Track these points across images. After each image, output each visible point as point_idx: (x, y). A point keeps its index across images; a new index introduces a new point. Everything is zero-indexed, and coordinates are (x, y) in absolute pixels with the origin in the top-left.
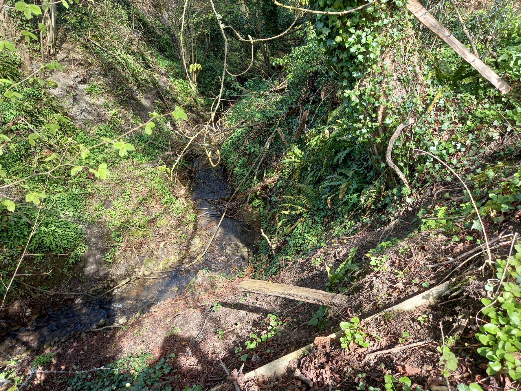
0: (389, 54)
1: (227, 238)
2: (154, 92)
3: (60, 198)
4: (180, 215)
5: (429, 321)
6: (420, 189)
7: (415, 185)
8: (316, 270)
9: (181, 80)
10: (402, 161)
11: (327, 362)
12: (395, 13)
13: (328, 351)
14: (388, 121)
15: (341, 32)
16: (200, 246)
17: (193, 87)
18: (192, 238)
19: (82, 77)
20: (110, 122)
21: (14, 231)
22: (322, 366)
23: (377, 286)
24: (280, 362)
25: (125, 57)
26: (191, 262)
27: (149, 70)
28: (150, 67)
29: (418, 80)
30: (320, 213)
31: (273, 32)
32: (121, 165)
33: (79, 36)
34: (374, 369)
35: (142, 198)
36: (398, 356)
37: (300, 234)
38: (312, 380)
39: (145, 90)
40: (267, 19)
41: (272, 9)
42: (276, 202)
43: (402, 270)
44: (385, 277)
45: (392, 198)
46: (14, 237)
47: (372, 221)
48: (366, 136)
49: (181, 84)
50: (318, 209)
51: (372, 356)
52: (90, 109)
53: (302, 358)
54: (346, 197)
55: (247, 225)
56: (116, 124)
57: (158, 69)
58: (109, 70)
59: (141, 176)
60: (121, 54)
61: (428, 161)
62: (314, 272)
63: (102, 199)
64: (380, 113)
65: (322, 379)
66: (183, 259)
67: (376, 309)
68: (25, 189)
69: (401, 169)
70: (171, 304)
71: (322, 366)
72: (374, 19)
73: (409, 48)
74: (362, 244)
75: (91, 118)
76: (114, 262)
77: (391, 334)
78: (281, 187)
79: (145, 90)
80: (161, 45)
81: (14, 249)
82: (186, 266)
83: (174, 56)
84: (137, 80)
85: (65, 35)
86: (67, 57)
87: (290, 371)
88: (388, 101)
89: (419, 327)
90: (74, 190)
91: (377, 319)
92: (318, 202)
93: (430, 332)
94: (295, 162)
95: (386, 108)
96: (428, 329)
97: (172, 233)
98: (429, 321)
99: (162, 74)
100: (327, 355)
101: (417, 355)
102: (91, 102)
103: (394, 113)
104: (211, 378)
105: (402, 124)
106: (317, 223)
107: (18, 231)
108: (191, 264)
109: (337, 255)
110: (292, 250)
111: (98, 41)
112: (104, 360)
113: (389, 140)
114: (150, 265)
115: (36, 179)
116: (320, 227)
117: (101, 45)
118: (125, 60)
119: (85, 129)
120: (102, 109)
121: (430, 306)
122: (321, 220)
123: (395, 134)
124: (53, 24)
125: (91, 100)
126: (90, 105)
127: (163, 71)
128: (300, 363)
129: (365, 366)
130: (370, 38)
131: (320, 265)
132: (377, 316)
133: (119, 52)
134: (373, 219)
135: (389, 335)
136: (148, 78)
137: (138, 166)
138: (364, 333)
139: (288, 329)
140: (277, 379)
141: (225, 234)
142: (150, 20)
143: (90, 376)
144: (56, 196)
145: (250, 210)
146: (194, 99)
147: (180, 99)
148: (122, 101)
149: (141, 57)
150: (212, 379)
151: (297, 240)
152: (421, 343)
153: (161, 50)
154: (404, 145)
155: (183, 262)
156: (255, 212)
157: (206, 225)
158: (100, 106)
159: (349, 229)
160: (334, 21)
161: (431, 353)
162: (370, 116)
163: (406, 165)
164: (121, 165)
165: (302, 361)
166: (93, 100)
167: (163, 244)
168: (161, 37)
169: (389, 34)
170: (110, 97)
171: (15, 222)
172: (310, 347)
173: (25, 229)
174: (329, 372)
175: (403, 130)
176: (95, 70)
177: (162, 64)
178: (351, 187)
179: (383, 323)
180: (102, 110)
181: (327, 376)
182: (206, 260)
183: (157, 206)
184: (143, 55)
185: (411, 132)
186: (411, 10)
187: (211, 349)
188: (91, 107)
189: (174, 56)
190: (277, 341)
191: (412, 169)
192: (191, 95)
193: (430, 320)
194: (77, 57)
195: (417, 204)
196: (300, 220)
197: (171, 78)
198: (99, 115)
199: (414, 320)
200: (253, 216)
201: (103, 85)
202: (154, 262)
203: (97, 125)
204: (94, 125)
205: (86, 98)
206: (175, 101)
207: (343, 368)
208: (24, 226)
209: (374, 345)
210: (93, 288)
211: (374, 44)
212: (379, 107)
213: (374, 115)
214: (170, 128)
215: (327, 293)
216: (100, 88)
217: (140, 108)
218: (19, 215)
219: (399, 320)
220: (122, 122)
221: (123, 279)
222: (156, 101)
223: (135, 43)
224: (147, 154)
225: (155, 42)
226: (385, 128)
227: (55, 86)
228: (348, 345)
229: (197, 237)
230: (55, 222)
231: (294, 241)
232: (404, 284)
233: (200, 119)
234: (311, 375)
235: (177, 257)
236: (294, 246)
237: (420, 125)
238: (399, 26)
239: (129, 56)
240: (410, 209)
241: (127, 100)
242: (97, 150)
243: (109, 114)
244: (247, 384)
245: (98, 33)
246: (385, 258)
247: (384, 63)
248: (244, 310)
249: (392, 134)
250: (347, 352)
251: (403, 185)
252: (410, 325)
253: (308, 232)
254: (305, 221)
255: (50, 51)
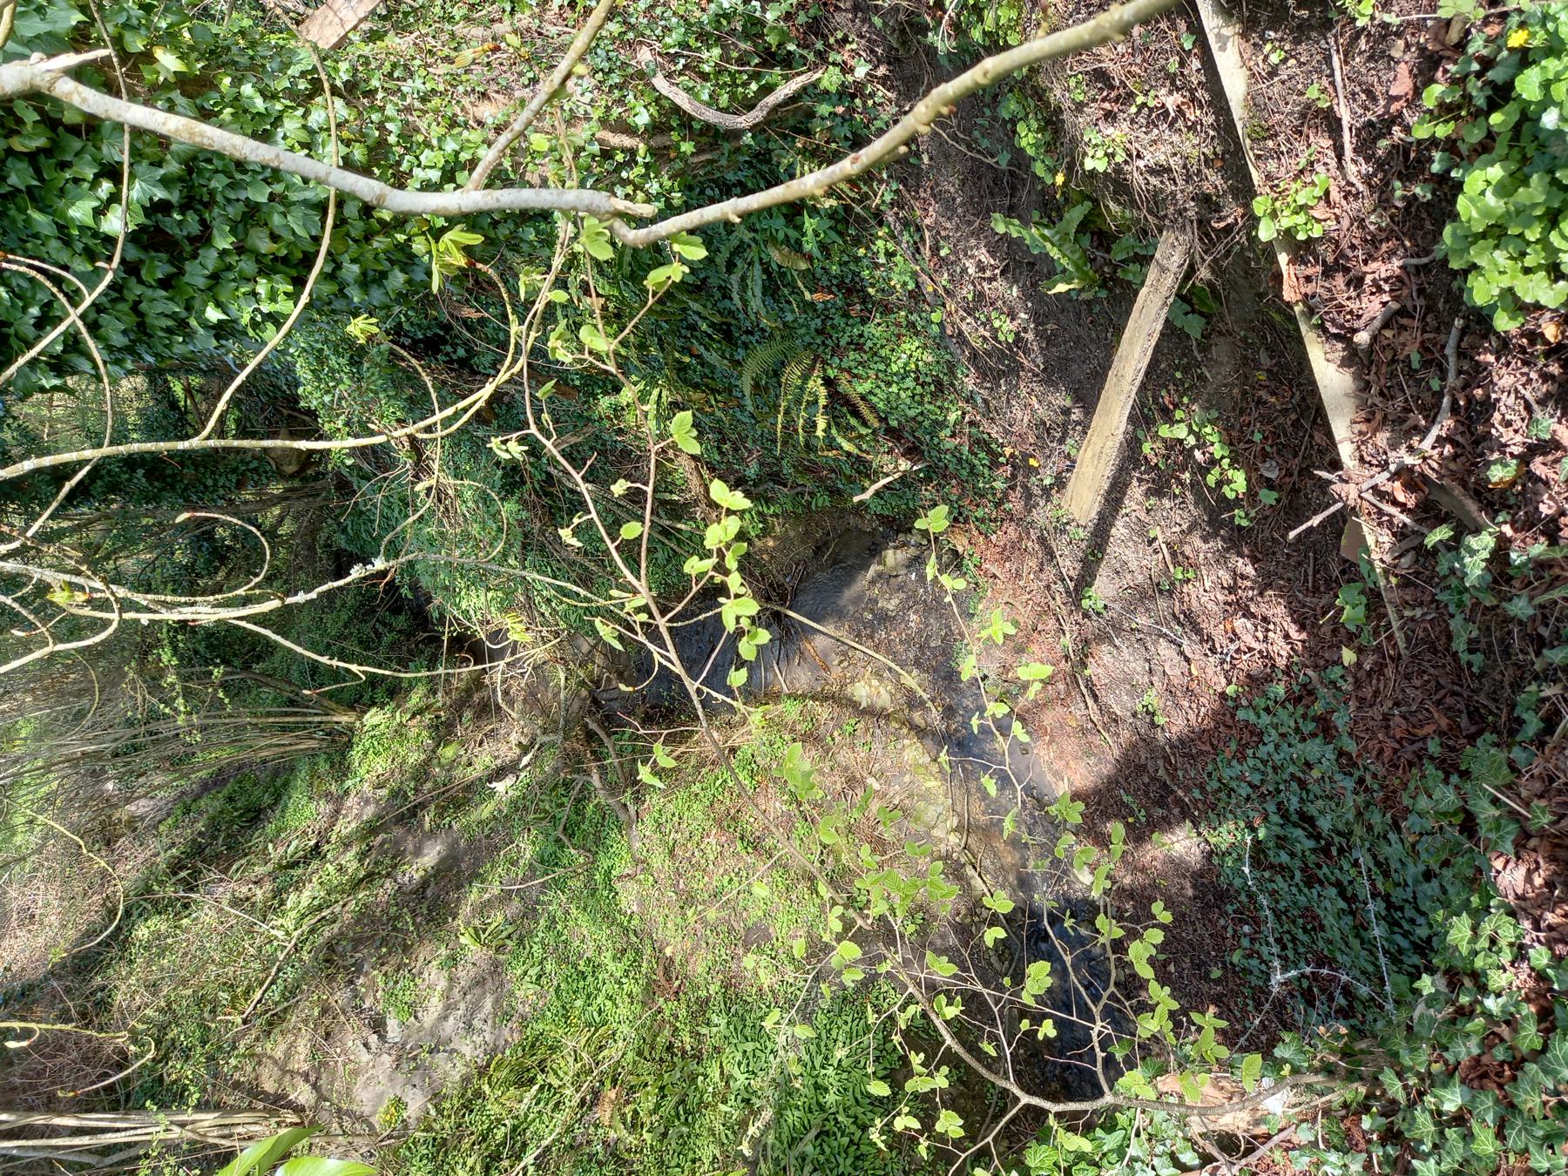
0: (468, 106)
1: (851, 608)
2: (398, 831)
3: (739, 1064)
4: (787, 737)
5: (1282, 40)
6: (832, 40)
7: (819, 54)
8: (1025, 330)
9: (356, 754)
10: (745, 84)
11: (1346, 270)
12: (363, 85)
13: (1319, 269)
14: (642, 119)
15: (401, 238)
16: (875, 683)
17: (375, 721)
18: (854, 705)
19: (366, 1032)
20: (500, 949)
21: (841, 1169)
22: (1357, 282)
23: (1163, 157)
24: (1327, 382)
25: (293, 914)
26: (922, 703)
27: (326, 847)
28: (317, 846)
29: (528, 30)
30: (833, 327)
31: (213, 472)
32: (635, 908)
33: (235, 1048)
34: (1380, 165)
35: (739, 843)
36: (1360, 111)
37: (889, 384)
38: (1384, 304)
39: (394, 857)
40: (173, 488)
41: (141, 472)
42: (761, 464)
43: (1131, 95)
44: (1142, 136)
45: (839, 120)
46: (855, 1169)
47: (890, 177)
48: (668, 184)
49: (365, 754)
50: (819, 332)
51: (1351, 169)
52: (462, 1006)
53: (1325, 330)
54: (807, 247)
55: (816, 553)
56: (505, 934)
57: (322, 824)
58: (336, 959)
59: (671, 853)
60: (284, 928)
61: (758, 14)
62: (1030, 336)
63: (741, 952)
64: (616, 140)
65: (1386, 280)
66: (914, 727)
67: (1231, 160)
68: (715, 1157)
69: (768, 89)
70: (1050, 742)
71: (1357, 282)
72: (382, 143)
73: (446, 51)
74: (963, 204)
75: (488, 1003)
76: (920, 908)
77: (1302, 125)
78: (719, 448)
79: (394, 857)
80: (241, 815)
81: (889, 1169)
82: (935, 716)
83: (273, 780)
84: (356, 884)
85: (237, 1085)
86: (306, 1077)
87: (1353, 358)
88: (588, 119)
89: (1292, 62)
90: (715, 1030)
91: (1258, 157)
92: (803, 331)
93: (1309, 38)
94: (658, 402)
95: (603, 122)
96: (1300, 43)
97: (839, 758)
98: (1282, 40)
99: (337, 812)
100: (1328, 273)
101: (1363, 70)
102: (441, 1005)
103: (621, 101)
104: (1306, 580)
105: (654, 81)
106: (861, 336)
107: (841, 1161)
108: (929, 704)
109: (988, 274)
110: (931, 407)
111: (247, 993)
112: (1202, 900)
113: (691, 118)
114: (931, 813)
115: (685, 1129)
116: (875, 330)
117: (261, 985)
118: (303, 916)
119: (524, 1017)
120: (461, 973)
121: (1244, 35)
122: (853, 326)
123: (678, 101)
124: (211, 1116)
125: (435, 1005)
126: (449, 1008)
127: (325, 808)
128: (1337, 337)
129: (1370, 185)
130: (427, 156)
131: (1013, 319)
132: (1250, 156)
133: (280, 934)
134: (885, 176)
135: (1305, 129)
136: (354, 850)
137: (637, 862)
138: (1294, 186)
139: (1199, 394)
140: (1367, 387)
141: (840, 614)
142: (158, 851)
143: (1246, 929)
144: (736, 1072)
145: (771, 543)
146: (413, 716)
147: (414, 758)
148: (433, 919)
149: (290, 872)
150: (1310, 579)
151: (903, 395)
152: (1336, 61)
153: (255, 816)
154: (704, 77)
155: (923, 725)
156: (778, 529)
157: (814, 668)
158: (451, 980)
159: (898, 243)
160: (376, 257)
161: (1363, 40)
162: (621, 166)
163: (756, 76)
164: (635, 908)
165: (1334, 330)
166: (435, 1000)
167: (870, 781)
168: (214, 818)
169: (417, 104)
170: (423, 953)
171: (815, 1170)
172: (1303, 313)
173: (835, 1144)
174: (1373, 266)
175: (669, 76)
176: (341, 997)
177: (304, 814)
178: (781, 236)
179: (1270, 144)
180: (464, 974)
181: (1382, 269)
182: (917, 663)
183: (761, 800)
184: (281, 867)
185: (673, 58)
186: (334, 40)
187: (1221, 598)
188: (456, 1003)
189: (273, 780)
190: (1228, 419)
191: (771, 58)
192: (401, 725)
193: (1279, 35)
194: (303, 1048)
195: (872, 51)
196: (844, 386)
197: (349, 783)
198: (479, 982)
199: (1273, 73)
200: (792, 534)
201: (385, 974)
202: (922, 804)
203: (509, 986)
204: (512, 994)
205: (428, 1019)
206: (421, 773)
207: (1370, 233)
208: (825, 1147)
209: (1325, 164)
210: (994, 960)
211: (451, 146)
212: (601, 142)
213: (620, 157)
214: (509, 780)
215: (1148, 282)
216: (396, 982)
217: (451, 869)
218: (793, 1161)
219: (1271, 106)
220: (497, 919)
221: (969, 884)
222: (427, 826)
223: (244, 889)
224: (599, 841)
225: (229, 836)
226: (656, 128)
227: (399, 1103)
228: (1318, 221)
229: (849, 689)
230: (814, 1067)
231: (908, 401)
232: (1171, 92)
233: (476, 698)
234: (1373, 307)
235: (907, 742)
236: (921, 403)
237: (658, 32)
238: (396, 75)
239: (289, 904)
240: (882, 70)
241: (432, 903)
242: (590, 979)
243: (474, 952)
244: (1368, 459)
245: (225, 995)
246: (1091, 135)
247: (490, 121)
248: (1112, 525)
249: (676, 109)
250: (1332, 224)
251: (815, 85)
252: (1283, 83)
253: (886, 361)
254: (849, 371)
255: (292, 1124)
